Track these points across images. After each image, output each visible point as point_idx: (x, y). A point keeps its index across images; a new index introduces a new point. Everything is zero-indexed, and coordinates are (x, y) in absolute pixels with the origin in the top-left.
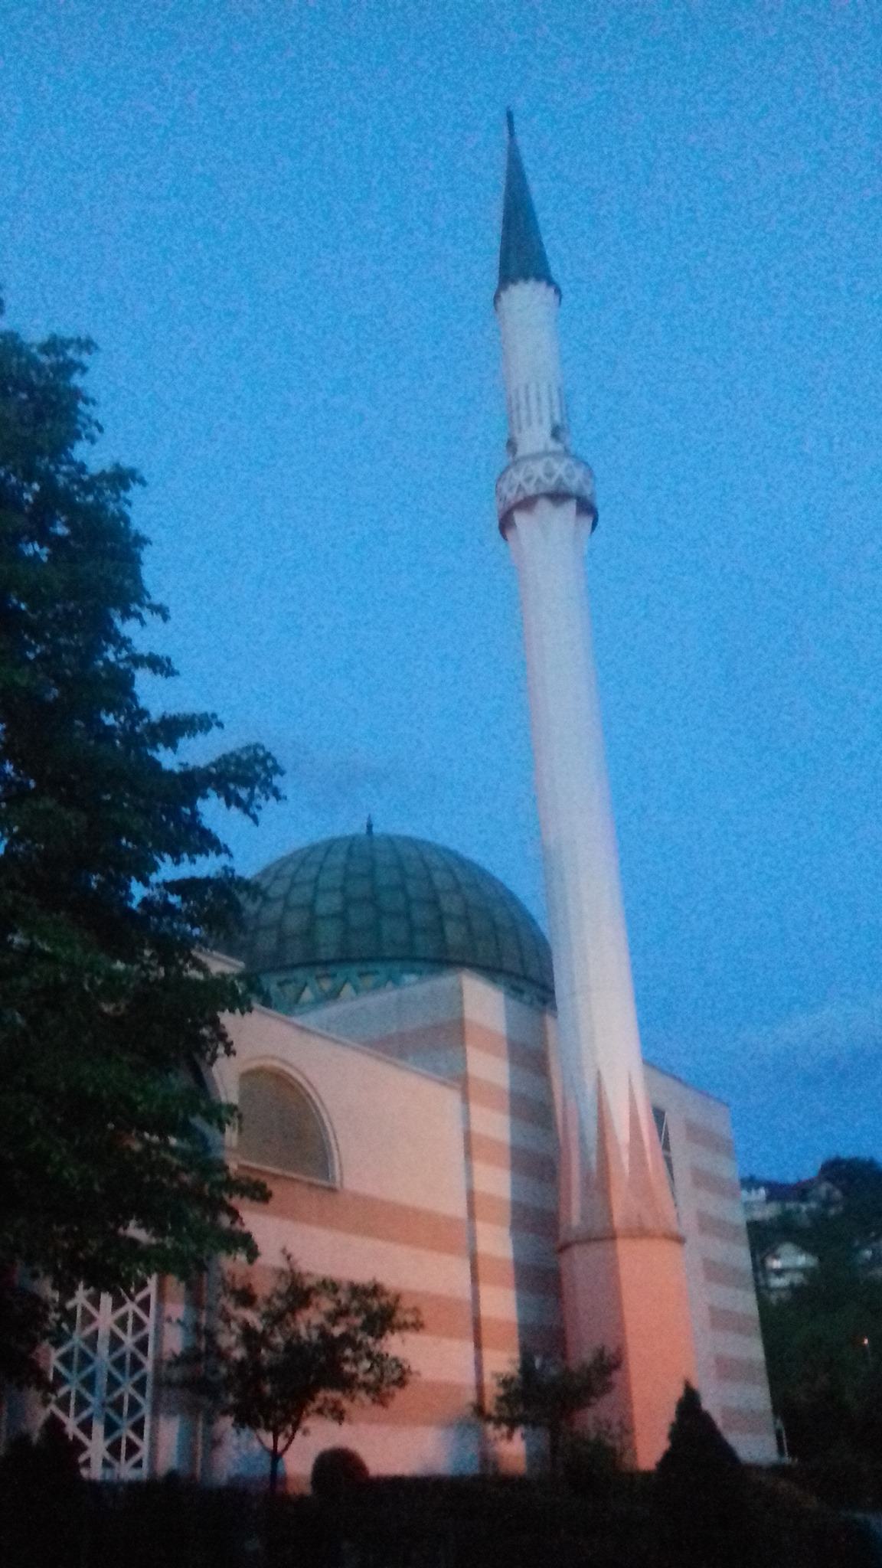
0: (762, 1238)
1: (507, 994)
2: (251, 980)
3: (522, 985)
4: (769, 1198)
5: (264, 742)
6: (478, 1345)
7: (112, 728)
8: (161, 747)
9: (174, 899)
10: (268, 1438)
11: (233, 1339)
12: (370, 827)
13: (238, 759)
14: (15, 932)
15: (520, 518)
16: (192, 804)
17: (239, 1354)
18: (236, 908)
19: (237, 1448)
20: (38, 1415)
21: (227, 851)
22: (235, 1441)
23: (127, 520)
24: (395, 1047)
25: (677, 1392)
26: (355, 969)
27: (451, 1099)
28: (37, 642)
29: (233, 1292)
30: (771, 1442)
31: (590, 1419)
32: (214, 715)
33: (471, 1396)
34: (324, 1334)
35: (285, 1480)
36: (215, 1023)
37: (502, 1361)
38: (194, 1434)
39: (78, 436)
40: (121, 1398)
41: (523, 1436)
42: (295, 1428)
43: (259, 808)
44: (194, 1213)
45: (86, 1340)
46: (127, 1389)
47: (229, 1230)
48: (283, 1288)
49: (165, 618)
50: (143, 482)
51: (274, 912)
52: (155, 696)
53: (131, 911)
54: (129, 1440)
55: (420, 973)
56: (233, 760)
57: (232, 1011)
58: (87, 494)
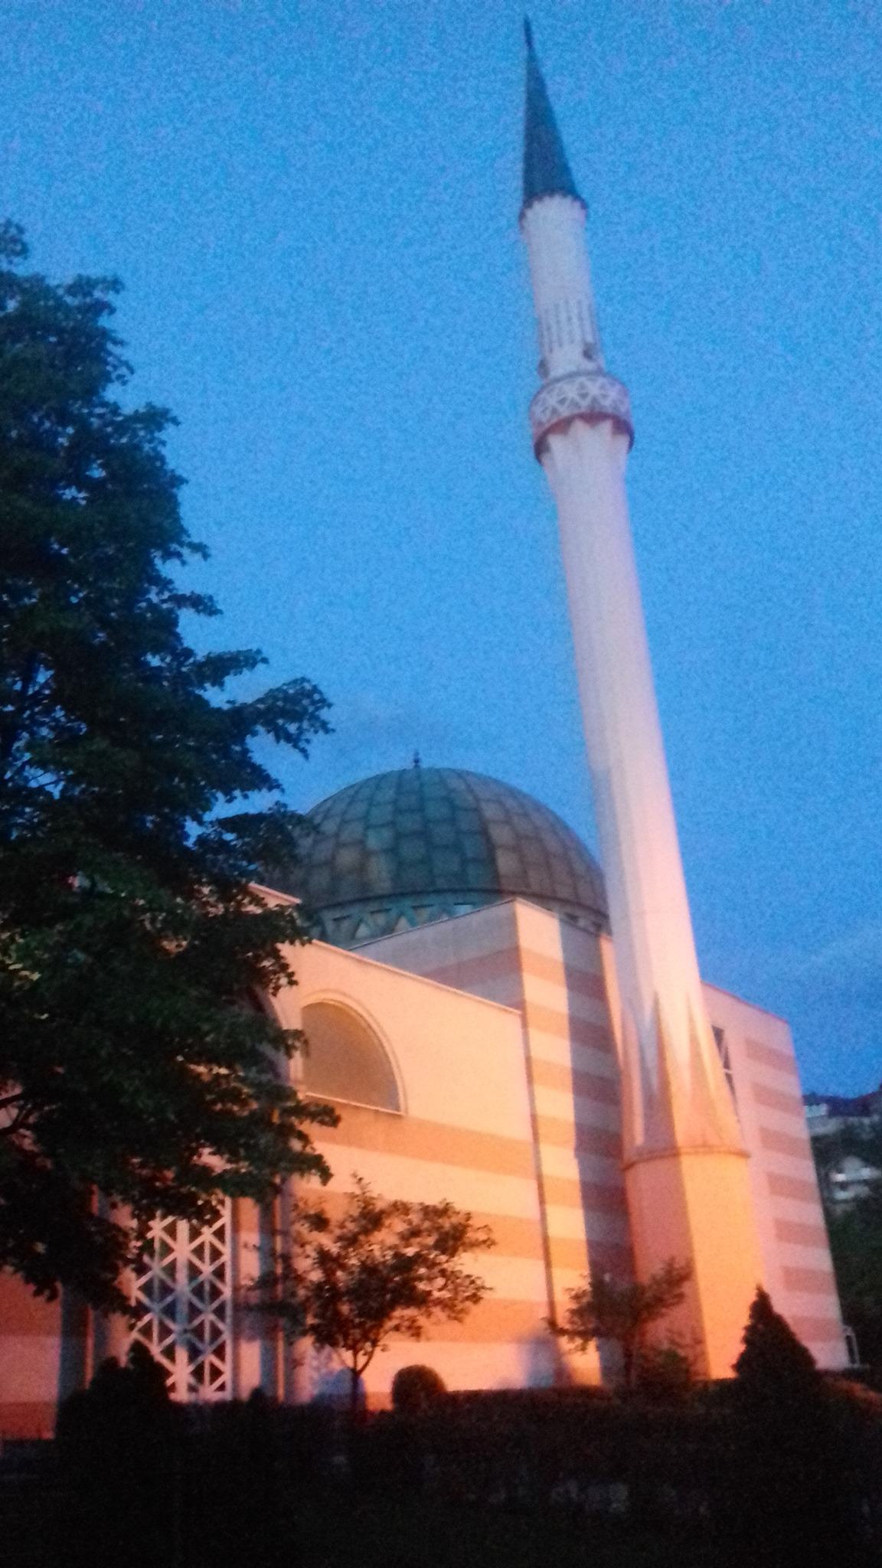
0: (826, 1153)
1: (561, 920)
2: (308, 911)
3: (578, 912)
4: (832, 1113)
5: (308, 676)
6: (548, 1265)
7: (159, 668)
8: (207, 685)
9: (229, 837)
10: (347, 1355)
11: (309, 1261)
12: (417, 761)
13: (285, 692)
14: (75, 875)
15: (555, 442)
16: (242, 742)
17: (316, 1276)
18: (290, 842)
19: (317, 1369)
20: (122, 1342)
21: (278, 786)
22: (315, 1363)
23: (162, 459)
24: (456, 975)
25: (752, 1297)
26: (408, 902)
27: (507, 1023)
28: (81, 585)
29: (307, 1217)
30: (842, 1347)
31: (659, 1331)
32: (259, 652)
33: (543, 1312)
34: (397, 1255)
35: (364, 1396)
36: (276, 955)
37: (574, 1277)
38: (275, 1357)
39: (109, 380)
40: (202, 1324)
41: (598, 1348)
42: (374, 1344)
43: (308, 741)
44: (264, 1140)
45: (164, 1269)
46: (209, 1317)
47: (301, 1154)
48: (356, 1212)
49: (206, 556)
50: (175, 421)
51: (323, 852)
52: (200, 636)
53: (187, 849)
54: (212, 1365)
55: (473, 904)
56: (281, 695)
57: (292, 943)
58: (121, 436)
